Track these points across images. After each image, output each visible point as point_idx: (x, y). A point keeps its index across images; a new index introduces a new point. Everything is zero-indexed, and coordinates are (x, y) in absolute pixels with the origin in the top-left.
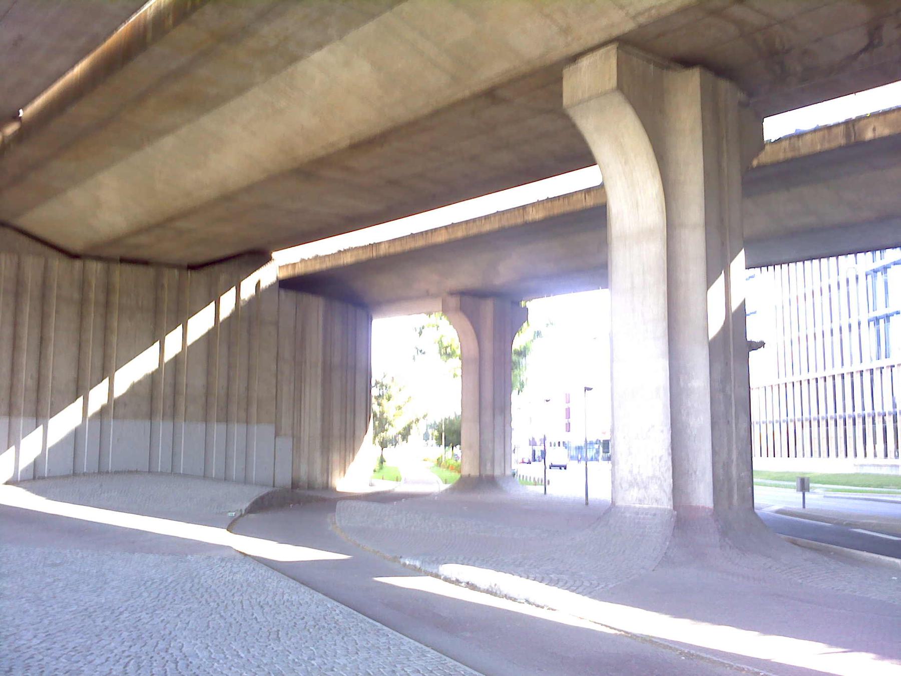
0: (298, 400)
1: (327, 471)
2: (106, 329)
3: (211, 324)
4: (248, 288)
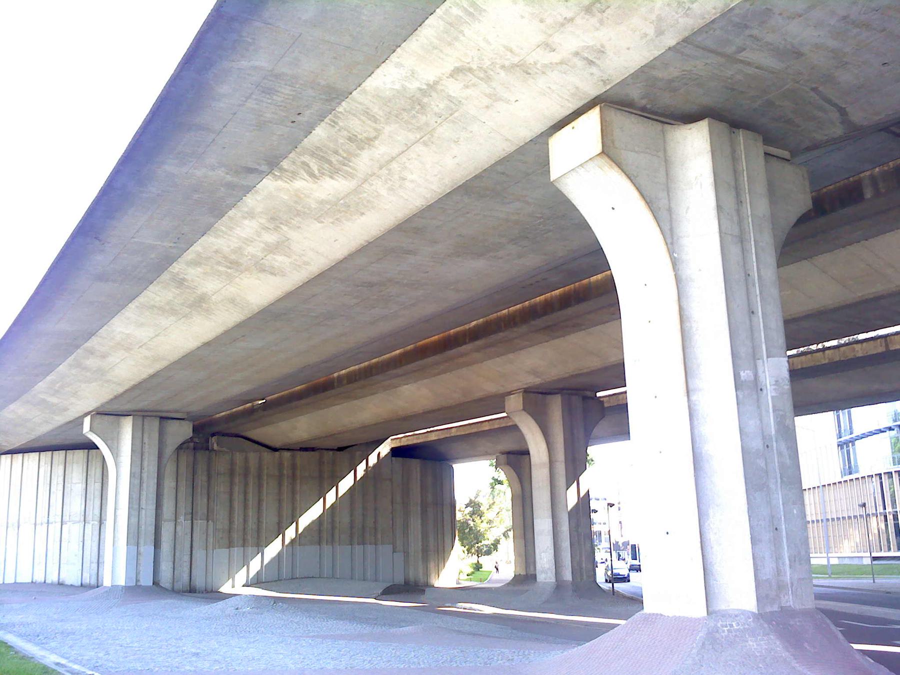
0: (406, 533)
1: (427, 574)
2: (293, 492)
3: (352, 483)
4: (373, 459)
